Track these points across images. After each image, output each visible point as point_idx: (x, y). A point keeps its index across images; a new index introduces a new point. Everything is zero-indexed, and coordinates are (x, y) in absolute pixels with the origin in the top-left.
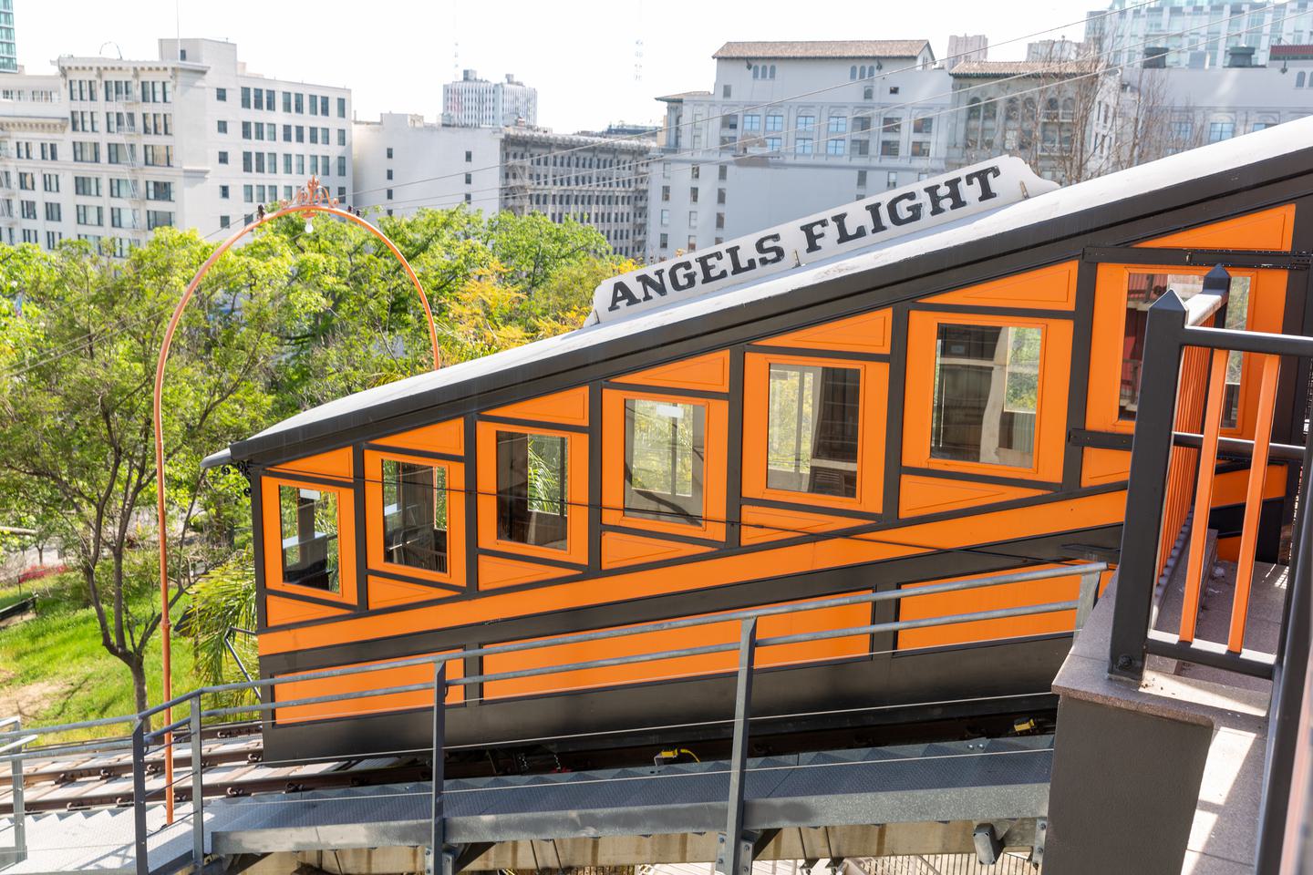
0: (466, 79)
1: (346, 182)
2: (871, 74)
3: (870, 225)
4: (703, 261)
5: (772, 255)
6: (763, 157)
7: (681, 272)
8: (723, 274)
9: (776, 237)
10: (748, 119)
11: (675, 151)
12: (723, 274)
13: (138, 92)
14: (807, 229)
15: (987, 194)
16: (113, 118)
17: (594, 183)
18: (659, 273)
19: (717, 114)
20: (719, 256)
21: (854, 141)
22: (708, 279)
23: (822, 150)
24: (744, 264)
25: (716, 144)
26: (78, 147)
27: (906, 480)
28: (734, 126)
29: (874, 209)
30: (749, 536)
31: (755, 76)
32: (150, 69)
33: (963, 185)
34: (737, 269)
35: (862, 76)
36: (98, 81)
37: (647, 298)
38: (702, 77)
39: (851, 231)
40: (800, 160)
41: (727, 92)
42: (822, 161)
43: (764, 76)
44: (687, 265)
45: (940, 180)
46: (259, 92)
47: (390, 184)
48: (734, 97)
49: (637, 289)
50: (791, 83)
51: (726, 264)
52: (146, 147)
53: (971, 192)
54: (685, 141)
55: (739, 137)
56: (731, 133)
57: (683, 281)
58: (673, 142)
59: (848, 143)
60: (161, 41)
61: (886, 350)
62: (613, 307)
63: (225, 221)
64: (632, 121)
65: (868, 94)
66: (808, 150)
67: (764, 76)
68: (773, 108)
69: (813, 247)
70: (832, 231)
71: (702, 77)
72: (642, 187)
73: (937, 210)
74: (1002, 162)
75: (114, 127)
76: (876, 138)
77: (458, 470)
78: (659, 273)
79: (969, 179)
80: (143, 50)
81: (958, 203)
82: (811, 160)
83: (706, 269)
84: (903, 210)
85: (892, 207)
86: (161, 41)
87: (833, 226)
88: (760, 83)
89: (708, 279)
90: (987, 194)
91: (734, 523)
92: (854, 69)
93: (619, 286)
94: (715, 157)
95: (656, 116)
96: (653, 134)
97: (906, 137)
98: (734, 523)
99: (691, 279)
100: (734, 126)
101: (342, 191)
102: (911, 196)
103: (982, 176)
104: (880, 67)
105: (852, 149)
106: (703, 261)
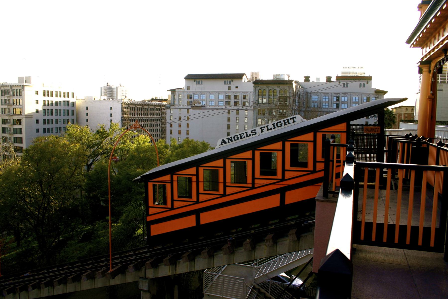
0: (107, 85)
1: (74, 117)
2: (230, 84)
3: (273, 127)
4: (240, 135)
5: (254, 133)
6: (200, 107)
7: (236, 137)
8: (244, 137)
9: (255, 130)
10: (195, 96)
11: (174, 105)
12: (244, 137)
13: (12, 93)
14: (261, 128)
15: (294, 122)
16: (4, 101)
17: (136, 115)
18: (231, 137)
19: (185, 94)
20: (243, 134)
21: (226, 102)
22: (241, 138)
23: (217, 104)
24: (249, 135)
25: (185, 103)
26: (3, 110)
27: (286, 172)
28: (191, 98)
29: (273, 124)
30: (256, 186)
31: (197, 84)
32: (15, 86)
33: (290, 120)
34: (247, 136)
35: (227, 84)
36: (11, 90)
37: (229, 142)
38: (182, 84)
39: (269, 128)
40: (211, 107)
41: (188, 88)
42: (217, 107)
43: (199, 84)
44: (237, 136)
45: (285, 119)
46: (48, 92)
47: (87, 117)
48: (191, 90)
49: (227, 141)
50: (208, 85)
51: (245, 135)
52: (13, 109)
53: (291, 121)
54: (177, 102)
55: (192, 101)
56: (190, 100)
57: (236, 139)
58: (173, 103)
59: (224, 102)
60: (19, 77)
61: (281, 149)
62: (222, 144)
63: (37, 130)
64: (159, 97)
65: (229, 88)
66: (213, 104)
67: (199, 84)
68: (202, 93)
69: (262, 132)
70: (266, 129)
71: (182, 84)
72: (164, 116)
73: (285, 125)
74: (296, 116)
75: (4, 103)
76: (234, 102)
77: (280, 153)
78: (231, 137)
79: (291, 119)
80: (15, 81)
81: (289, 123)
82: (214, 107)
83: (241, 136)
84: (279, 124)
85: (277, 124)
86: (19, 77)
87: (266, 128)
88: (198, 86)
89: (241, 138)
90: (294, 122)
91: (253, 183)
92: (225, 82)
93: (223, 140)
94: (186, 107)
95: (166, 95)
96: (165, 100)
97: (240, 100)
98: (253, 183)
99: (238, 138)
100: (191, 98)
101: (73, 120)
102: (280, 122)
103: (293, 118)
104: (232, 81)
105: (226, 104)
106: (240, 135)
